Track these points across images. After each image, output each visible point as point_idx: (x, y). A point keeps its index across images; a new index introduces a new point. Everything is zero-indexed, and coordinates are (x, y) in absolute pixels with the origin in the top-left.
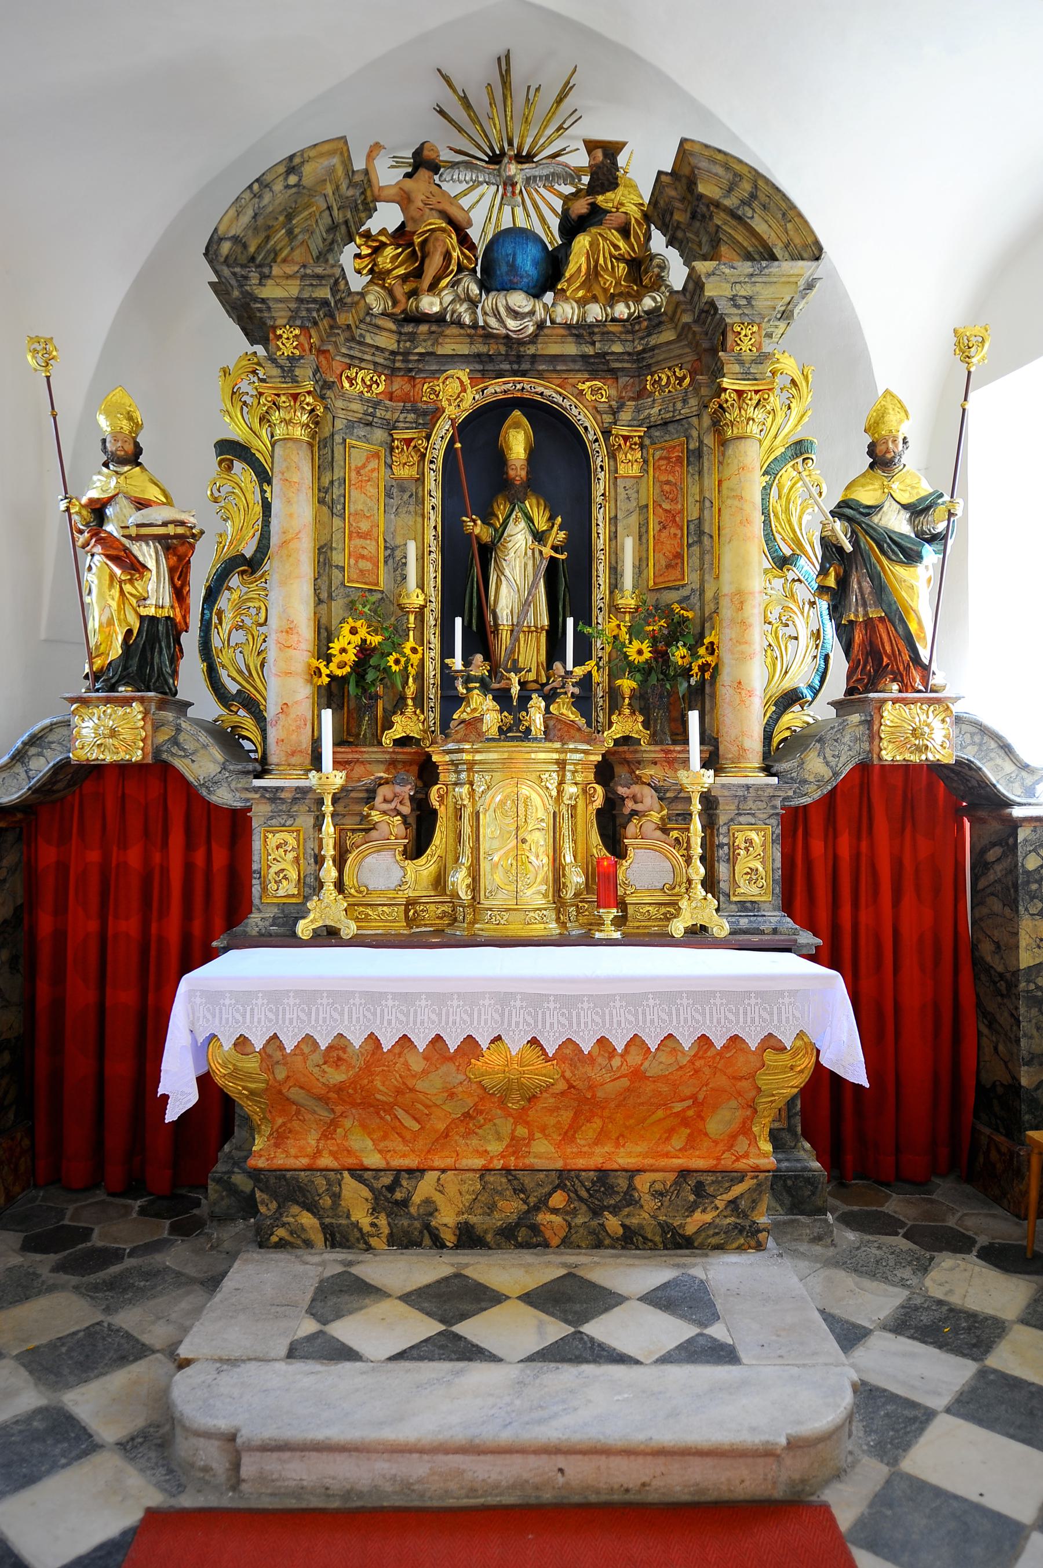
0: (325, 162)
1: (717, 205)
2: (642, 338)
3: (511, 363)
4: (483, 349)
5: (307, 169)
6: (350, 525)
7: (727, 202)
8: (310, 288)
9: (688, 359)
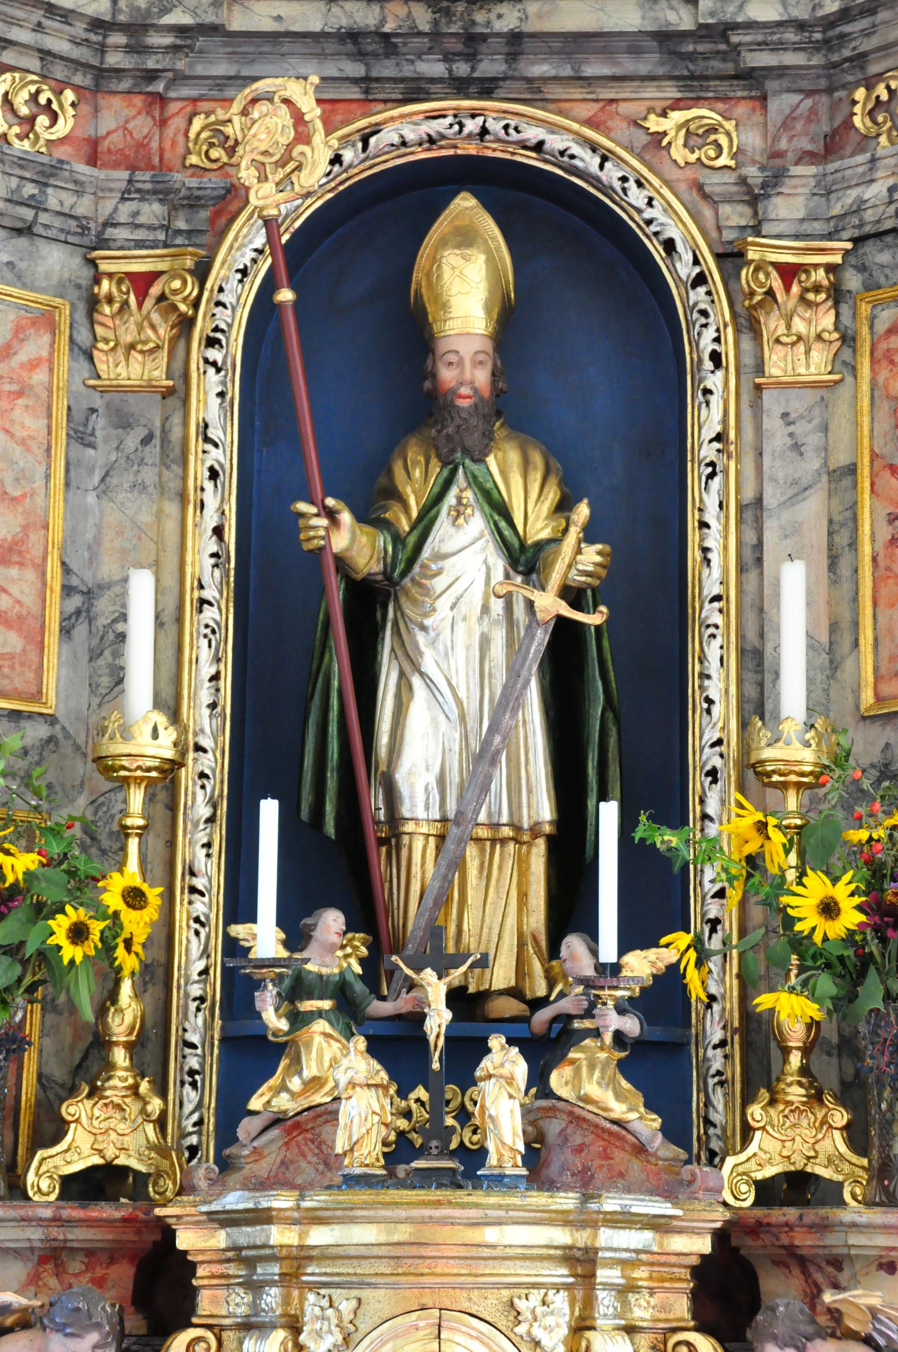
3: (448, 57)
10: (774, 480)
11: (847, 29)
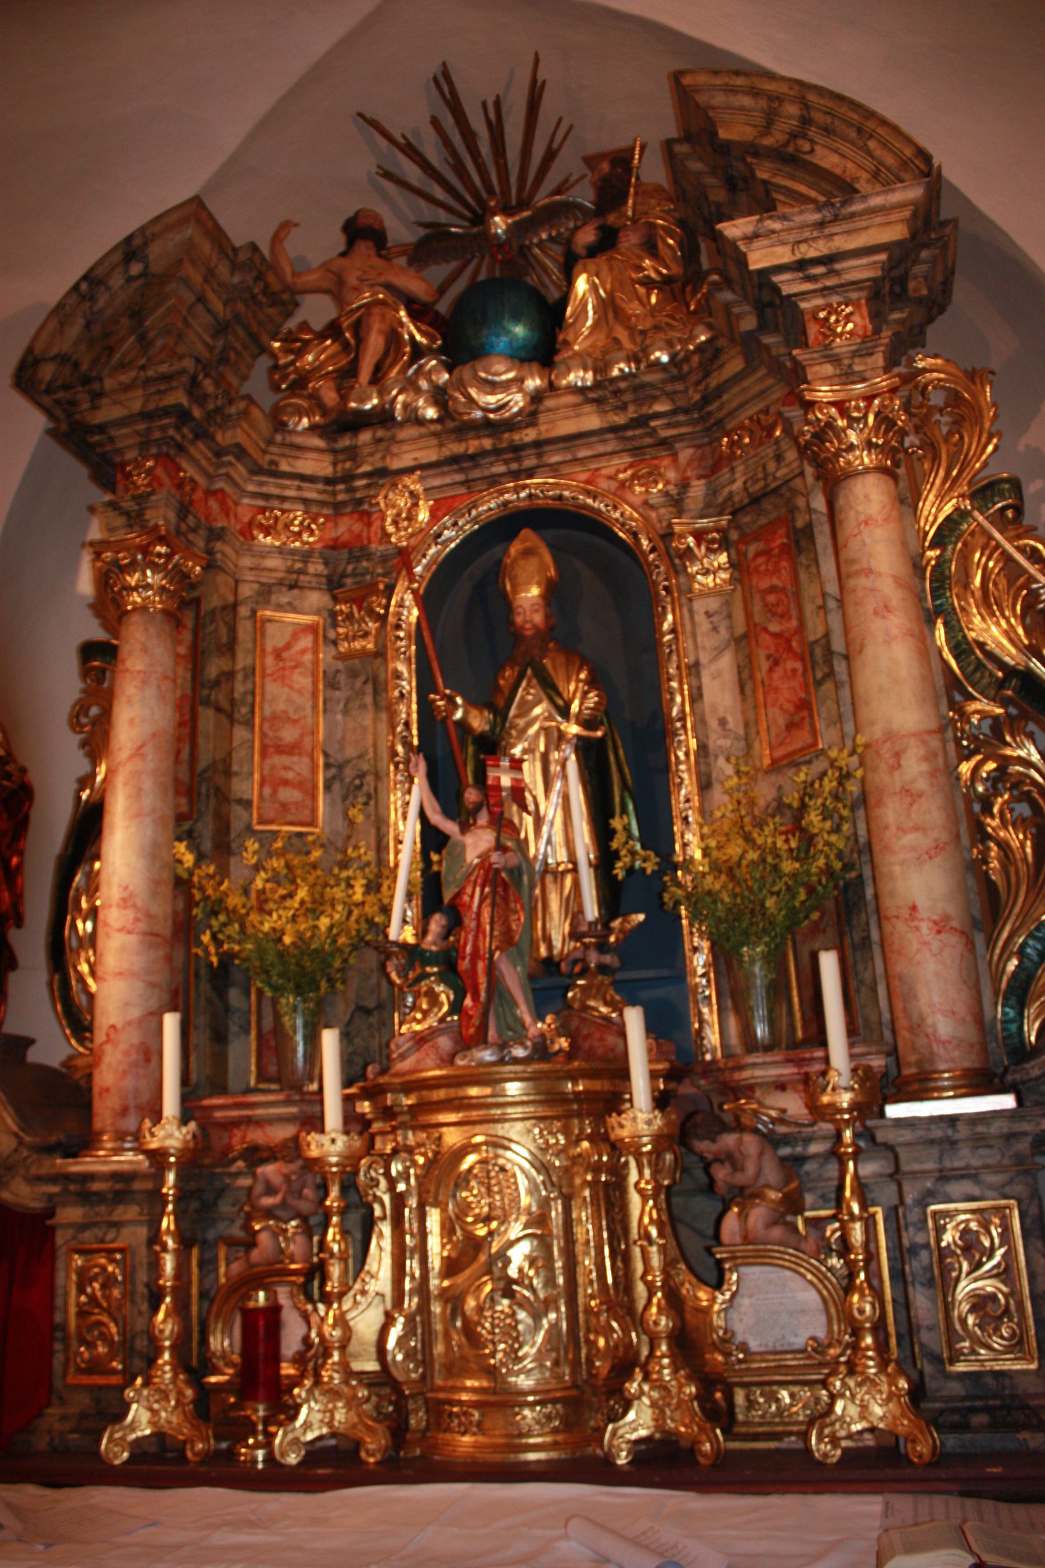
0: (178, 237)
1: (755, 150)
2: (698, 383)
3: (506, 462)
4: (457, 448)
5: (154, 251)
6: (263, 735)
7: (767, 141)
8: (157, 397)
9: (775, 396)
10: (704, 648)
11: (710, 408)
